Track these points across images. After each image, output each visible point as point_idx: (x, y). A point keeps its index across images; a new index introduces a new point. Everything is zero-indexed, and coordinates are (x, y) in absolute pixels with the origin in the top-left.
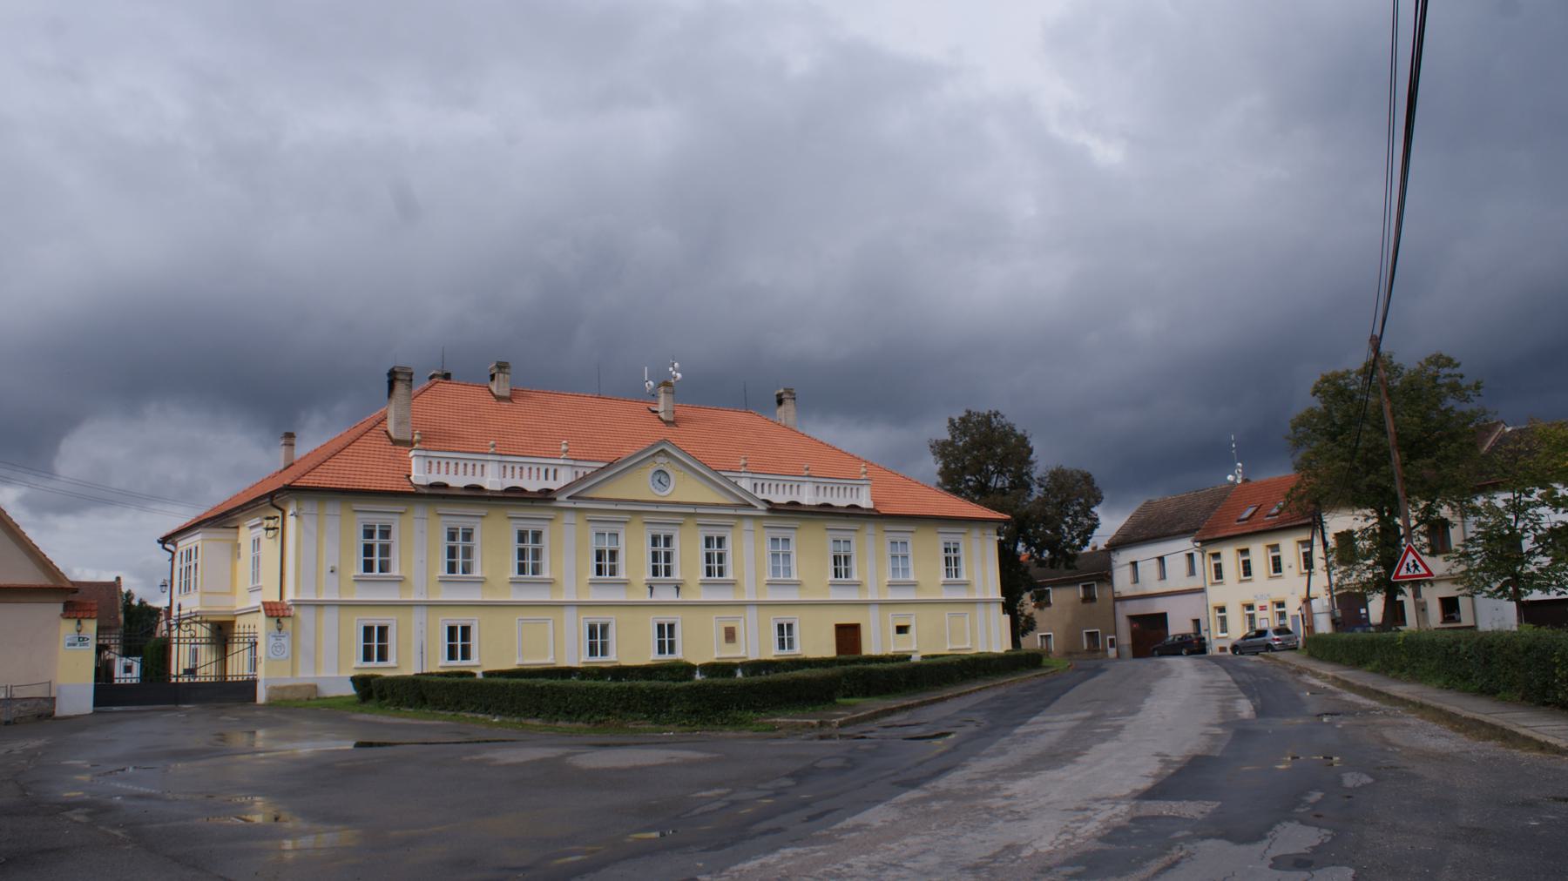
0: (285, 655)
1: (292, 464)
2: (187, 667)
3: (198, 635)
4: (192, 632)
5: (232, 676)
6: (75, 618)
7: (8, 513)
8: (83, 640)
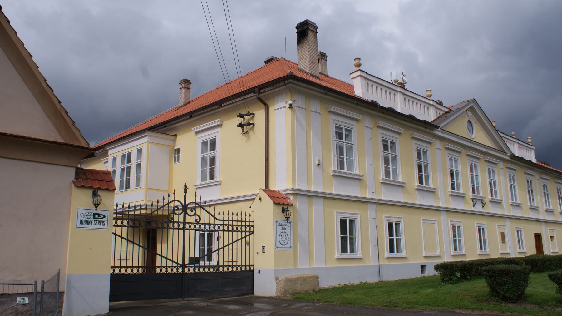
0: (288, 245)
1: (189, 103)
2: (192, 256)
3: (202, 221)
4: (197, 218)
5: (161, 267)
6: (91, 187)
7: (18, 35)
8: (99, 218)
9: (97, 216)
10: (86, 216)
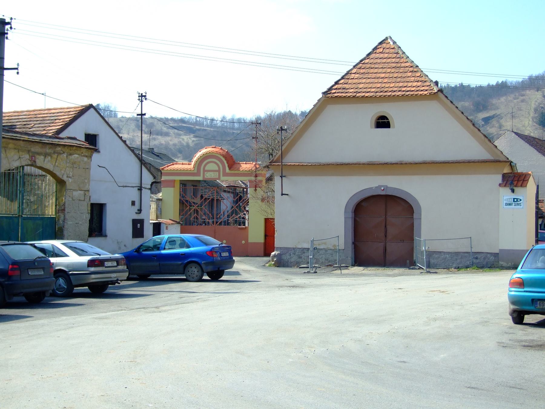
9: (515, 200)
10: (510, 201)
